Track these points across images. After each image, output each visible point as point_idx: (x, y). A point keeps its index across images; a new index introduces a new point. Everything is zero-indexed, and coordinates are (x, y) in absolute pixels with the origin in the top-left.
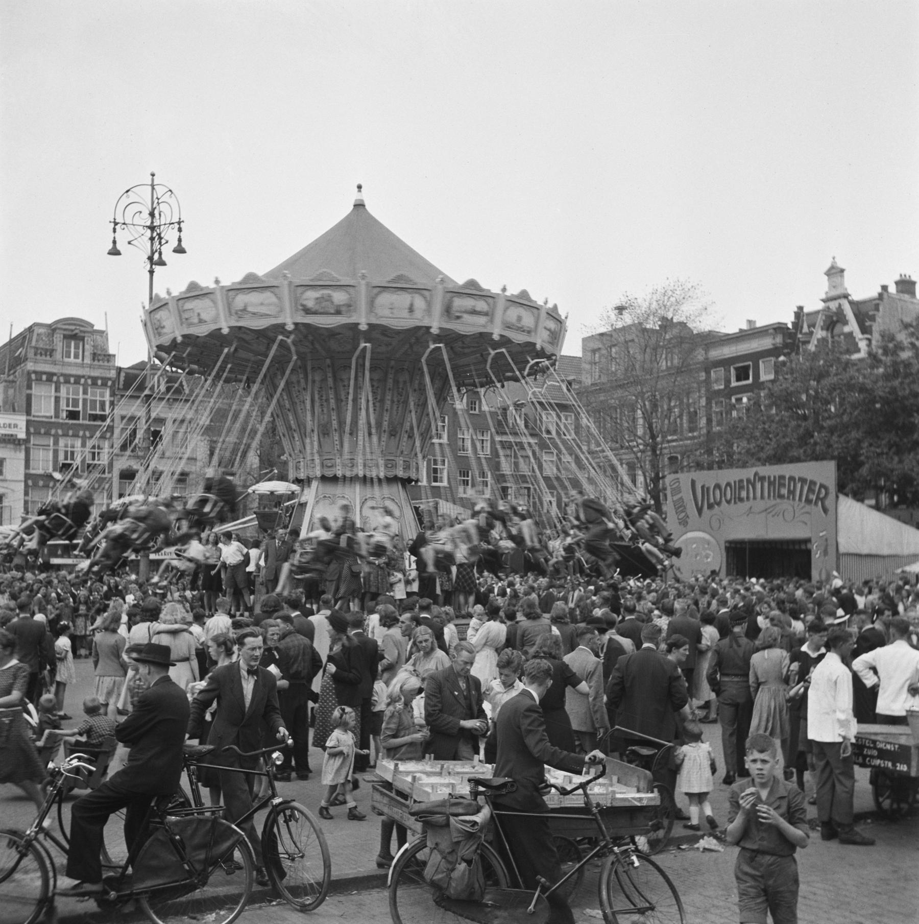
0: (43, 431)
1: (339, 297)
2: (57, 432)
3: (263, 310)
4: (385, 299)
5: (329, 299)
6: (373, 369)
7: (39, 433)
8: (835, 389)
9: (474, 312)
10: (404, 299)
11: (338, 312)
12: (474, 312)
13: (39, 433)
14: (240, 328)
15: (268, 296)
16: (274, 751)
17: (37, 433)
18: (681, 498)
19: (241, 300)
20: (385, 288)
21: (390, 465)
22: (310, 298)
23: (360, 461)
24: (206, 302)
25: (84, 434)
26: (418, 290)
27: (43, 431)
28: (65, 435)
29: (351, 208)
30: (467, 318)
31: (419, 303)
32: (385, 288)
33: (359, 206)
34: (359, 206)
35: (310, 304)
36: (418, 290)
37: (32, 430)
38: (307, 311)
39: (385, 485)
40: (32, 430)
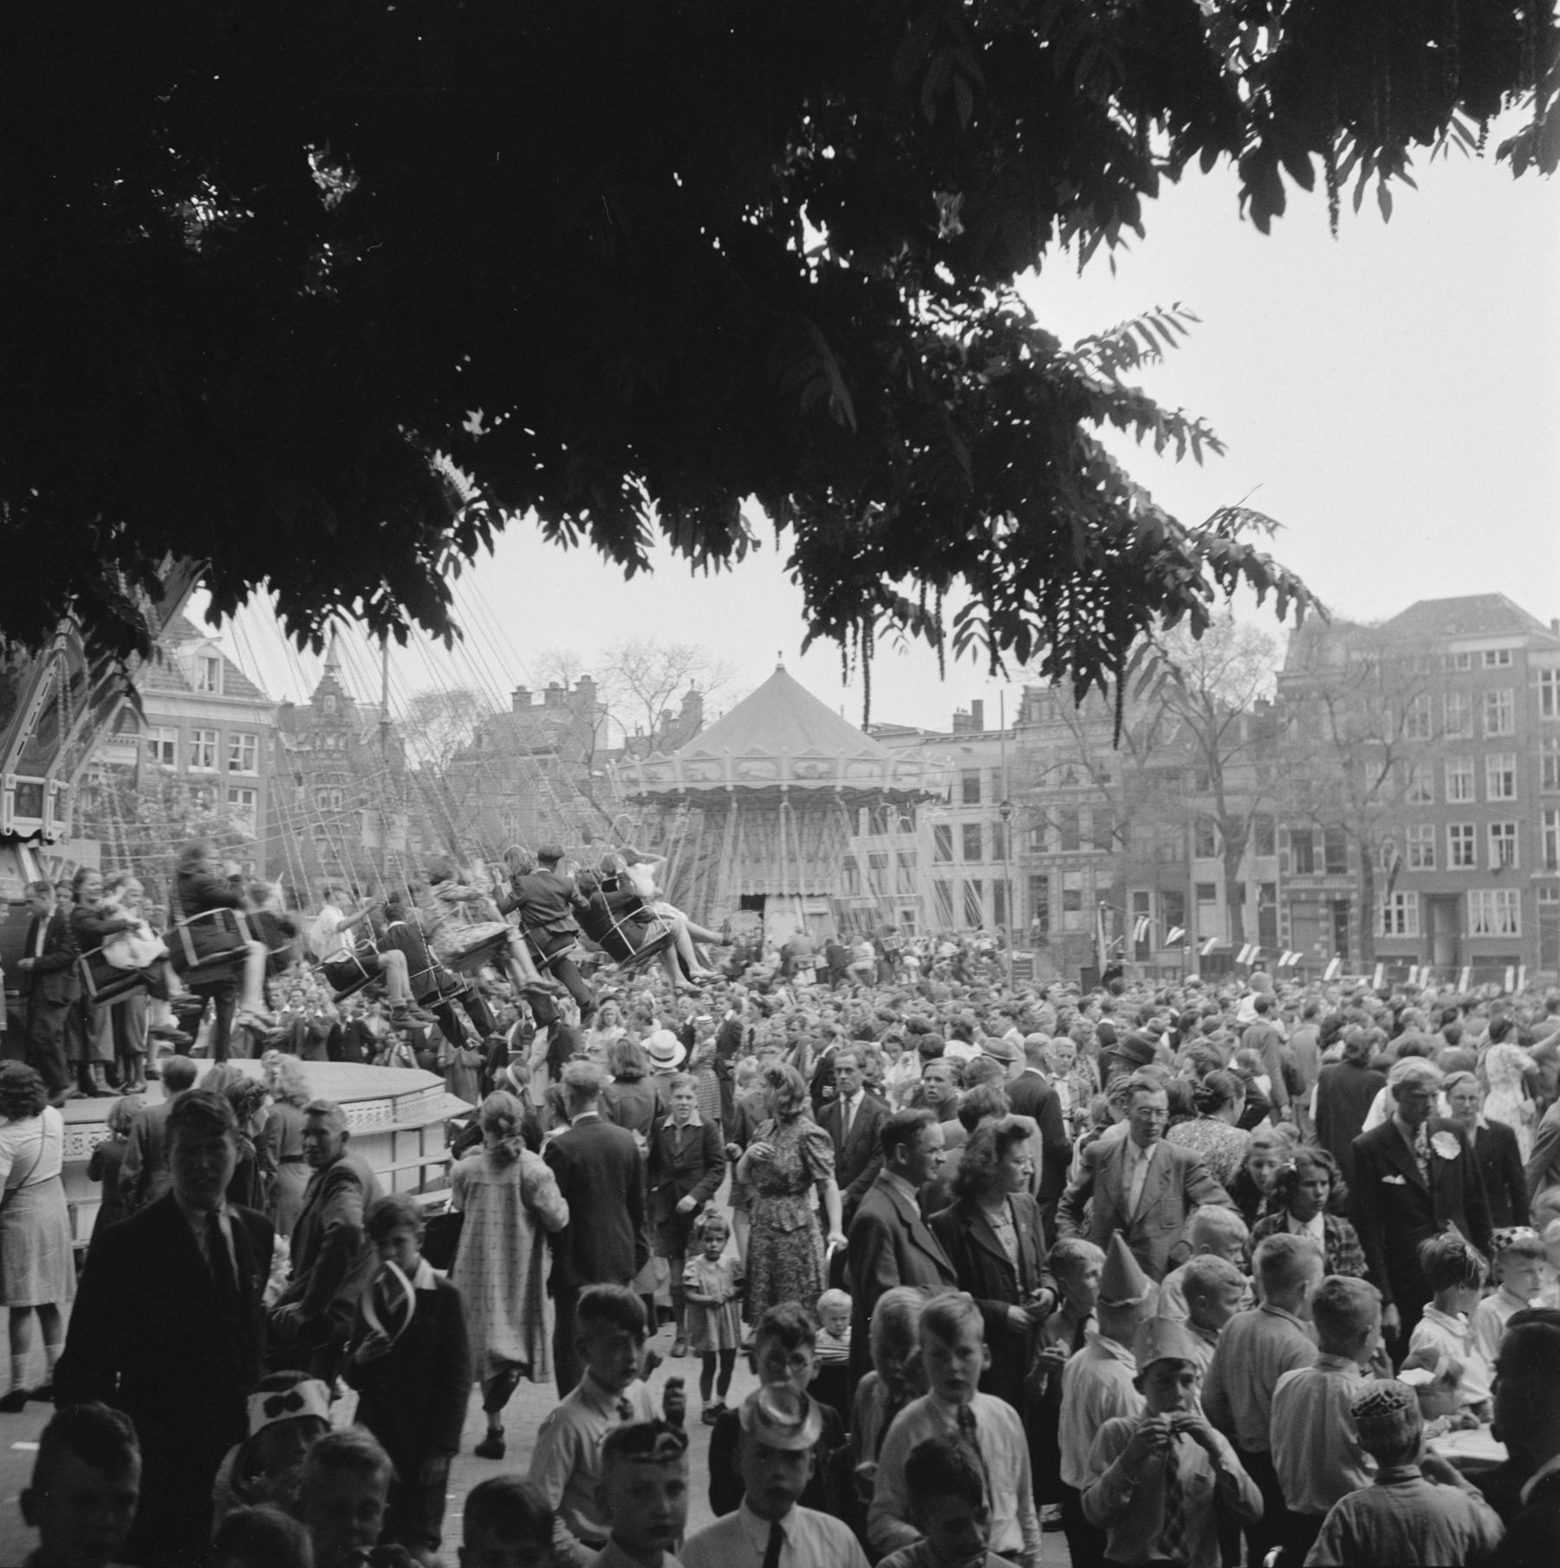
1: (822, 767)
3: (763, 774)
4: (855, 767)
5: (813, 767)
6: (1077, 847)
8: (1496, 872)
9: (909, 775)
10: (865, 768)
11: (820, 778)
12: (909, 775)
14: (744, 787)
15: (768, 765)
16: (257, 1175)
18: (537, 1151)
19: (745, 766)
20: (854, 760)
21: (809, 885)
22: (801, 767)
23: (802, 882)
24: (713, 765)
26: (876, 761)
29: (773, 671)
30: (906, 779)
31: (877, 770)
32: (854, 760)
33: (780, 669)
34: (780, 669)
35: (801, 771)
36: (876, 761)
38: (799, 777)
39: (805, 900)
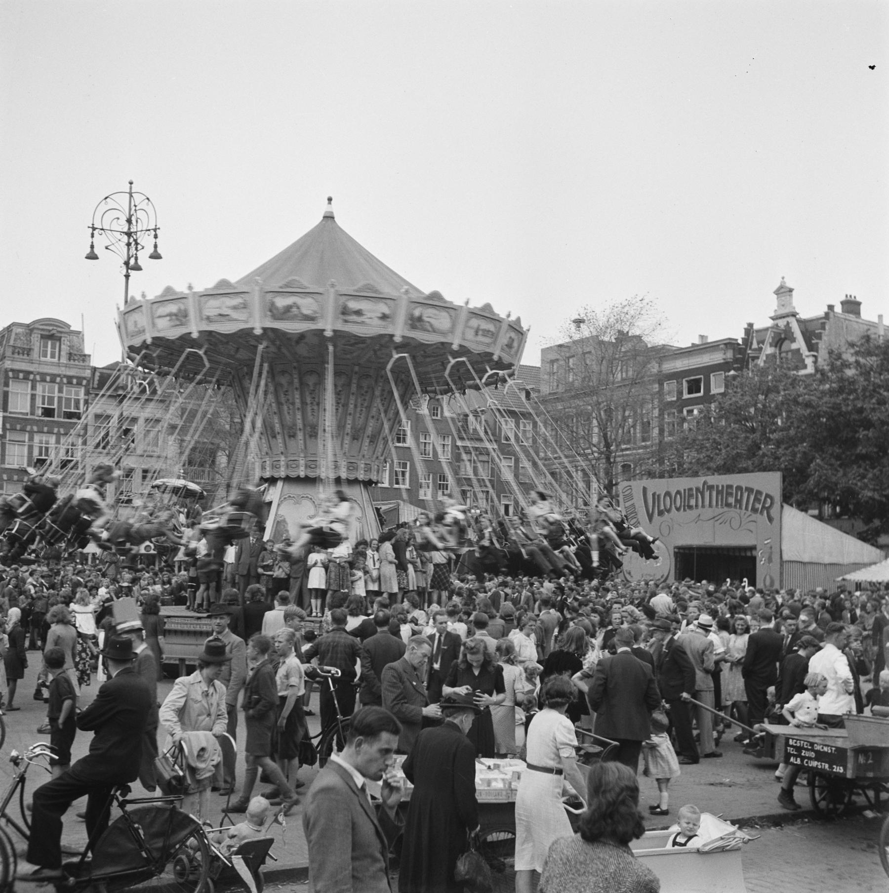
0: (18, 427)
2: (59, 431)
7: (16, 430)
13: (16, 430)
17: (13, 429)
25: (59, 431)
27: (18, 427)
28: (41, 432)
37: (8, 426)
40: (8, 426)
